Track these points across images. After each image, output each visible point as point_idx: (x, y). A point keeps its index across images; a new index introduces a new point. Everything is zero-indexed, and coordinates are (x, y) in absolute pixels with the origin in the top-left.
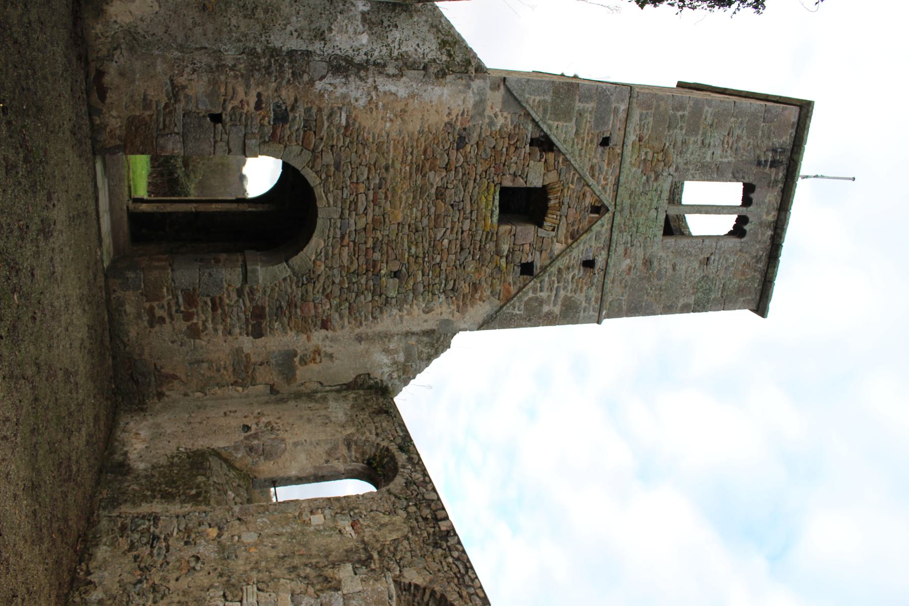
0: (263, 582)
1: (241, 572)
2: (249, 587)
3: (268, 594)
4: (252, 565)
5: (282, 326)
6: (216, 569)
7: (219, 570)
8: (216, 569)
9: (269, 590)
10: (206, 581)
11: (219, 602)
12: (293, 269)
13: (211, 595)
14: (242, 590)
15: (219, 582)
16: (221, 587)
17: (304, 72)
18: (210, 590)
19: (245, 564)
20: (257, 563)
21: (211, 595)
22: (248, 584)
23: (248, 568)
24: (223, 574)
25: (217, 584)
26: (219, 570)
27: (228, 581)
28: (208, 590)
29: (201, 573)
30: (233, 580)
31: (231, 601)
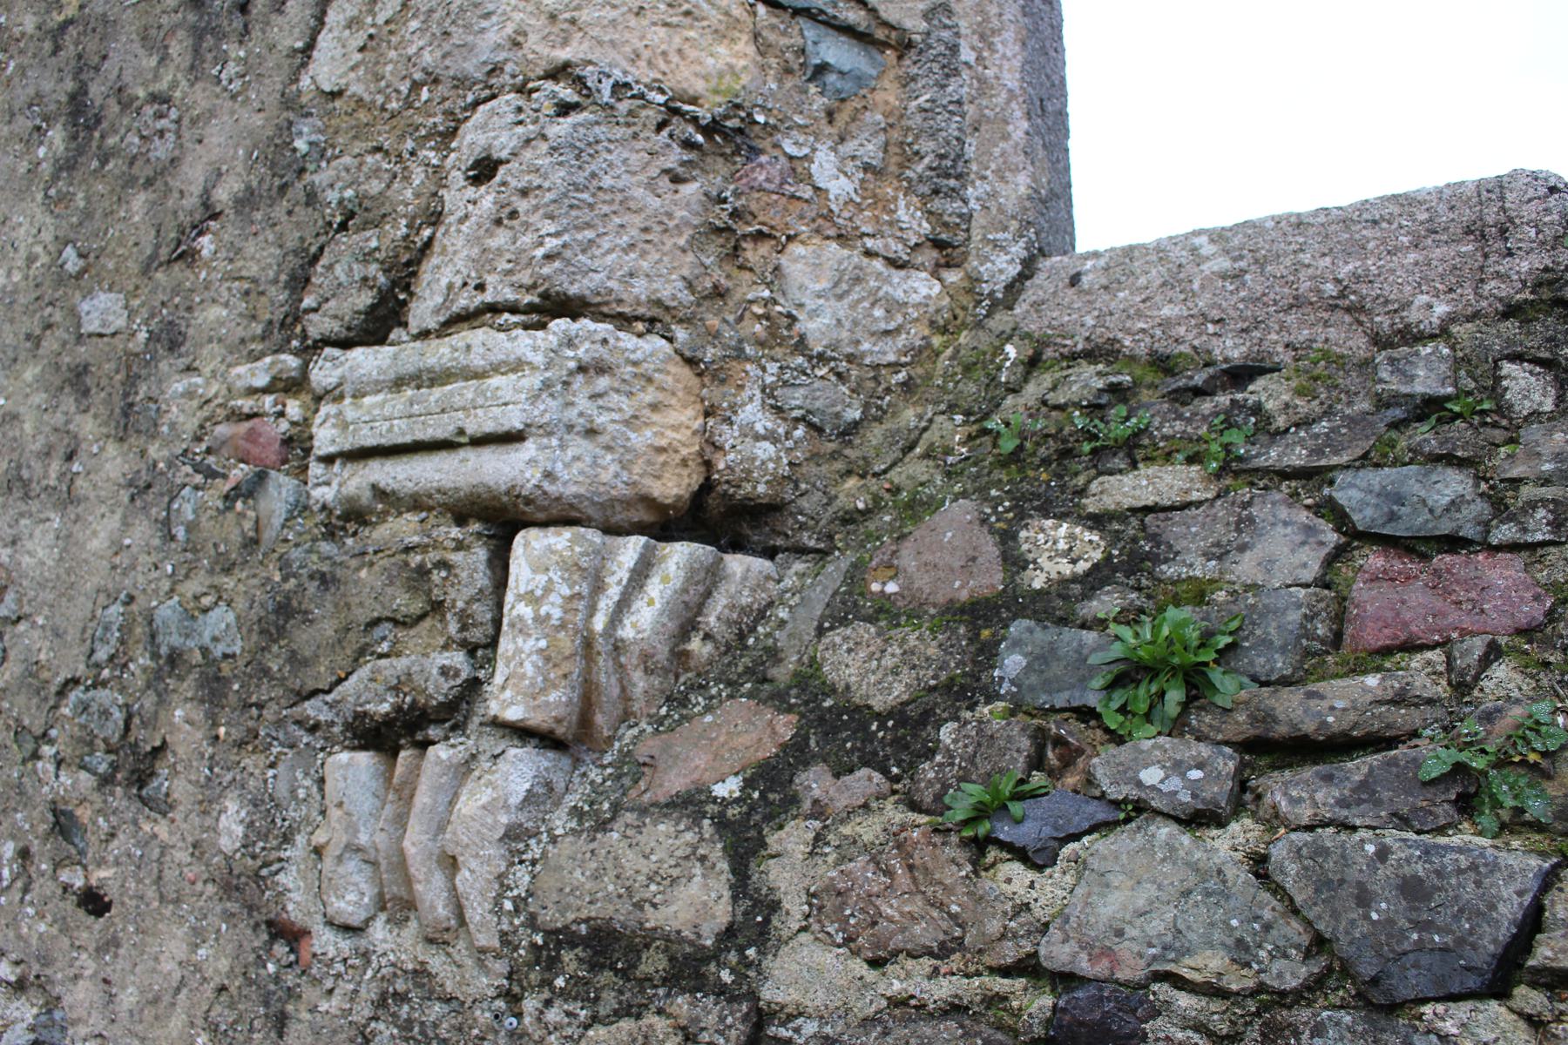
0: (299, 282)
1: (142, 533)
2: (325, 438)
3: (457, 195)
4: (87, 426)
5: (1040, 709)
6: (63, 824)
7: (73, 784)
8: (63, 824)
9: (407, 196)
10: (172, 947)
11: (472, 801)
12: (521, 733)
13: (350, 902)
14: (354, 515)
15: (208, 805)
16: (288, 778)
17: (750, 115)
18: (297, 907)
19: (67, 498)
20: (78, 380)
21: (350, 902)
22: (297, 445)
23: (115, 463)
24: (123, 745)
25: (231, 824)
26: (73, 784)
27: (213, 688)
28: (290, 934)
29: (80, 996)
30: (220, 620)
31: (483, 649)
